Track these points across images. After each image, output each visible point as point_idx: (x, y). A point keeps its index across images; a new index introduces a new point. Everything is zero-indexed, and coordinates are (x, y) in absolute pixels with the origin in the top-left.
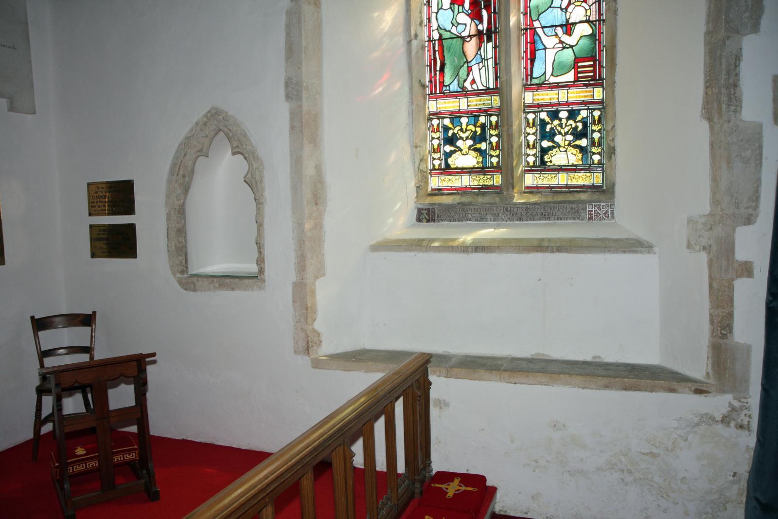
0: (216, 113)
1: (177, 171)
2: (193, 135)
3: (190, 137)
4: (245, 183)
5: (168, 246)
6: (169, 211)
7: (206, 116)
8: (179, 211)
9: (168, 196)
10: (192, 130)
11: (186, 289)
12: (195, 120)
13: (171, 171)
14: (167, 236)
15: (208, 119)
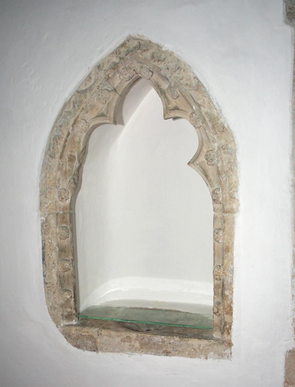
0: (139, 46)
1: (60, 150)
2: (91, 88)
3: (86, 91)
4: (213, 256)
5: (44, 276)
6: (47, 219)
7: (116, 52)
8: (64, 218)
9: (44, 193)
10: (89, 77)
11: (78, 347)
12: (96, 59)
13: (49, 150)
14: (43, 259)
15: (121, 59)
